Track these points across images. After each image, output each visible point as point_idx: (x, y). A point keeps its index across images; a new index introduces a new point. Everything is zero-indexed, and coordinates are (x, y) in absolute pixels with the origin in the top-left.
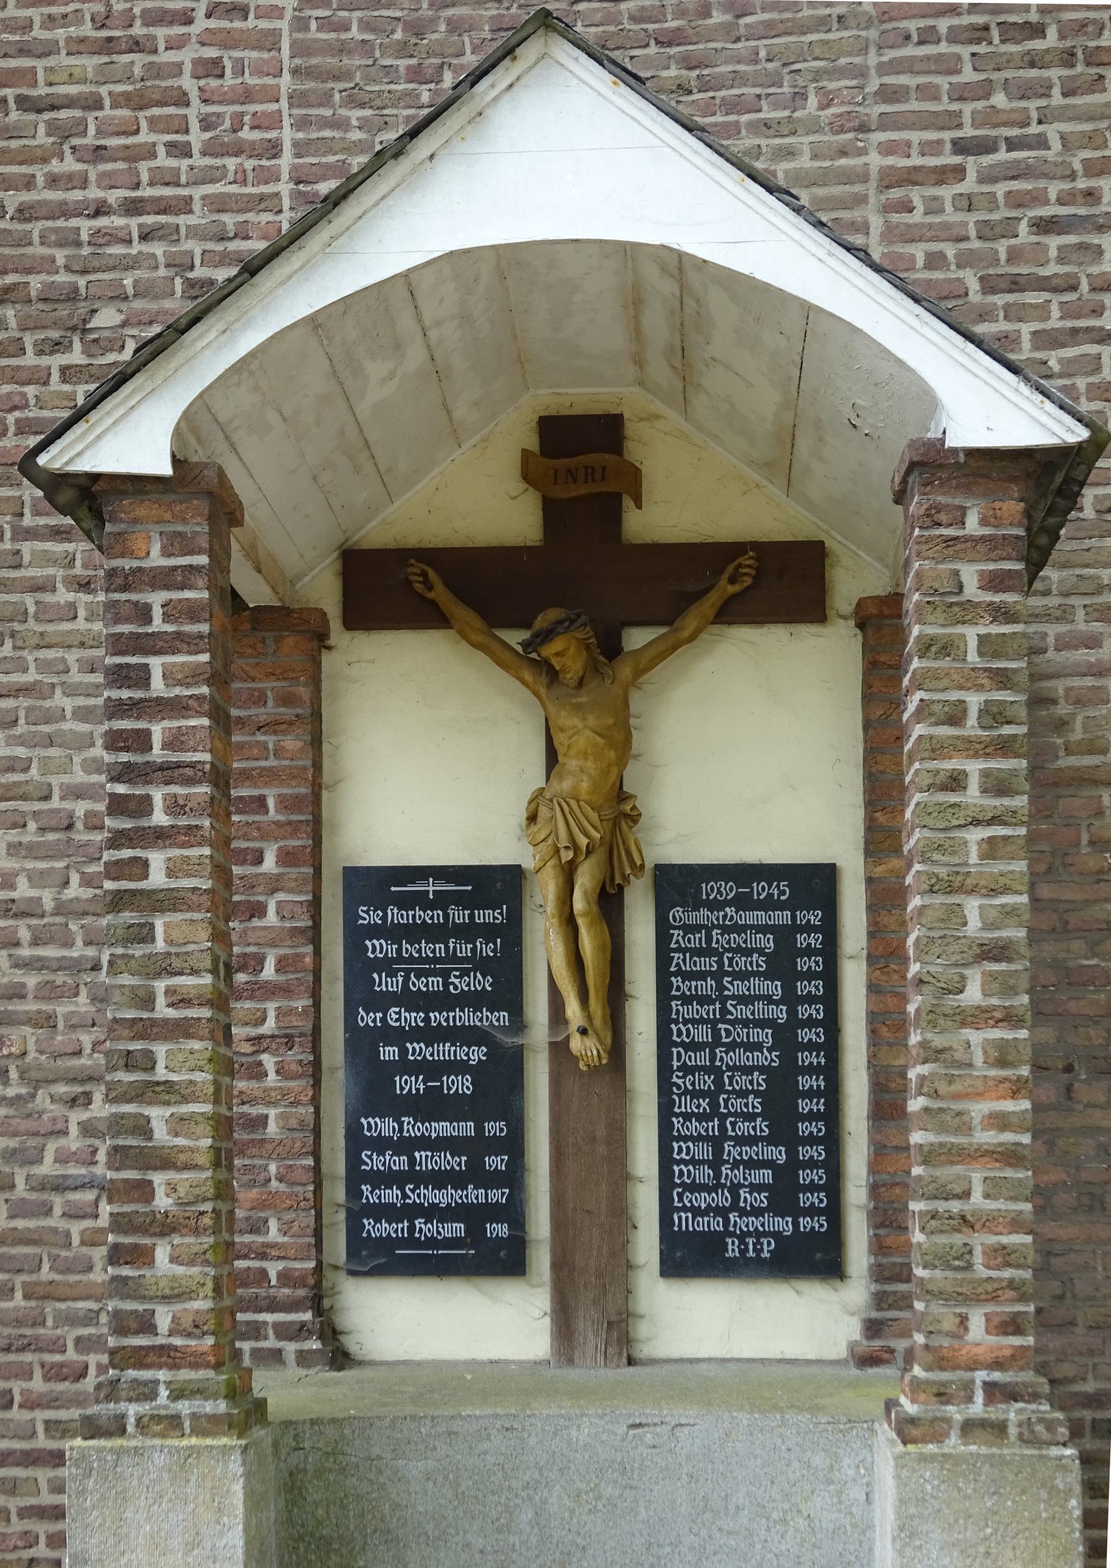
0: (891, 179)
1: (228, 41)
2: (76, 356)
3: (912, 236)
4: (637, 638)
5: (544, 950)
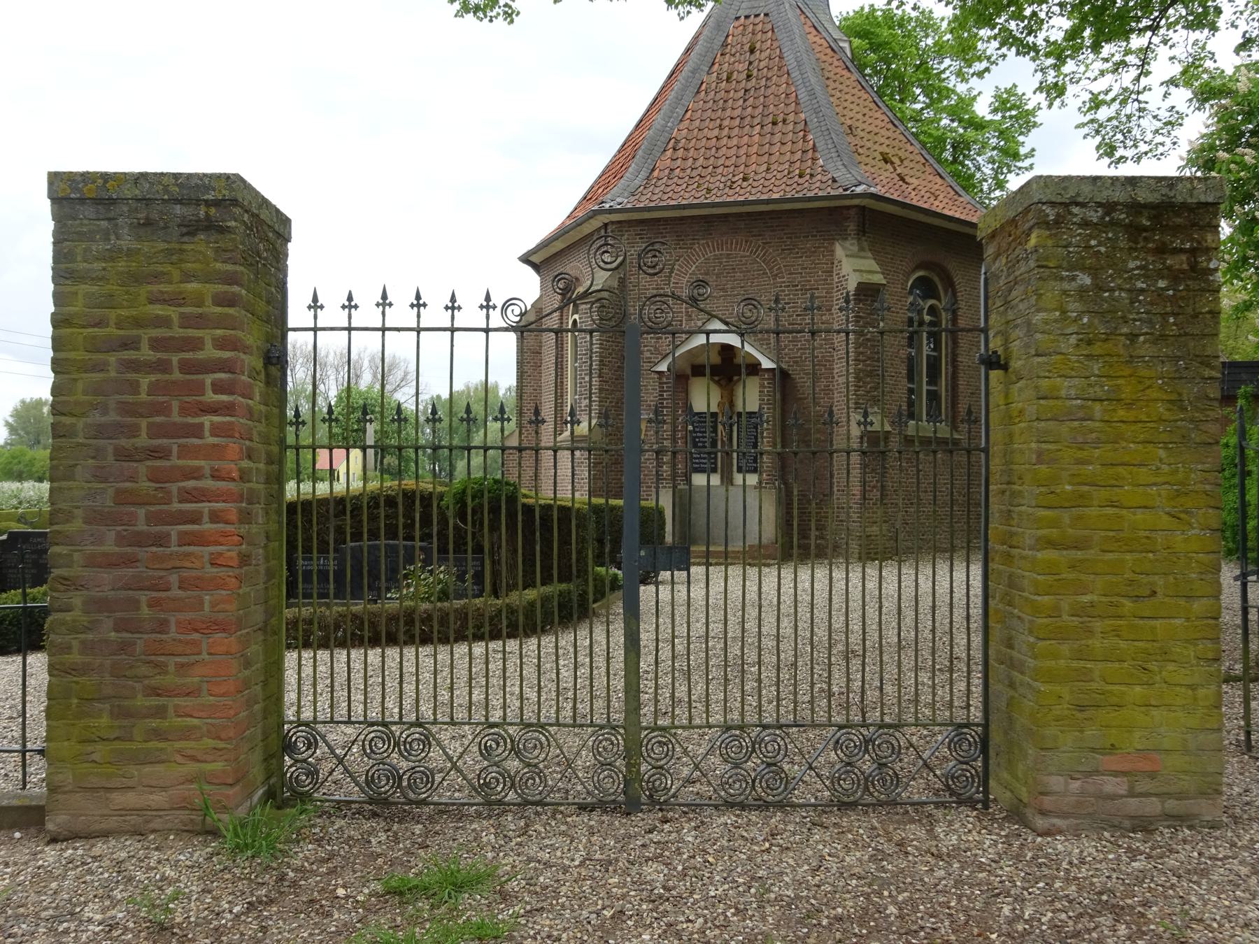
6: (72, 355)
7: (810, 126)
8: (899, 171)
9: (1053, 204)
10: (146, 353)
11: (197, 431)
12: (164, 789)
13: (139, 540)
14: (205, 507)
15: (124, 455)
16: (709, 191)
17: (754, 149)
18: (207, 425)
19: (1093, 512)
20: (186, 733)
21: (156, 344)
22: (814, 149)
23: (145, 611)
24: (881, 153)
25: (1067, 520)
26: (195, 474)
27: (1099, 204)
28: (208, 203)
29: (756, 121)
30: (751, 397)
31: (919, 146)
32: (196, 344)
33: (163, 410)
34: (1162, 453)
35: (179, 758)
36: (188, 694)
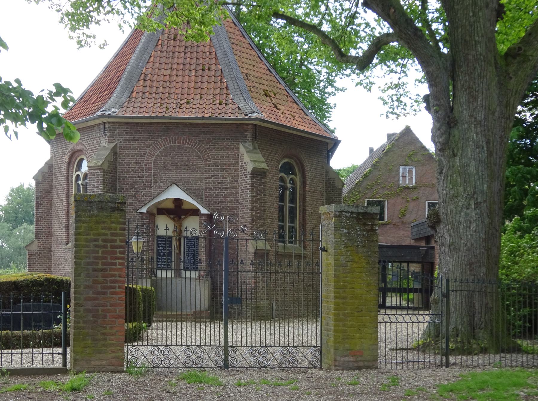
0: (206, 178)
1: (147, 163)
2: (133, 190)
3: (207, 183)
4: (183, 217)
5: (174, 244)
6: (80, 243)
7: (225, 74)
8: (274, 101)
9: (338, 212)
10: (101, 243)
11: (115, 264)
12: (106, 360)
13: (99, 293)
14: (117, 285)
15: (95, 270)
16: (167, 109)
17: (192, 85)
18: (117, 263)
19: (348, 290)
20: (112, 345)
21: (104, 241)
22: (227, 88)
23: (101, 313)
24: (264, 90)
25: (341, 292)
26: (114, 276)
27: (349, 212)
28: (118, 203)
29: (193, 67)
30: (192, 226)
31: (284, 84)
32: (115, 241)
33: (106, 258)
34: (364, 275)
35: (110, 352)
36: (112, 335)
